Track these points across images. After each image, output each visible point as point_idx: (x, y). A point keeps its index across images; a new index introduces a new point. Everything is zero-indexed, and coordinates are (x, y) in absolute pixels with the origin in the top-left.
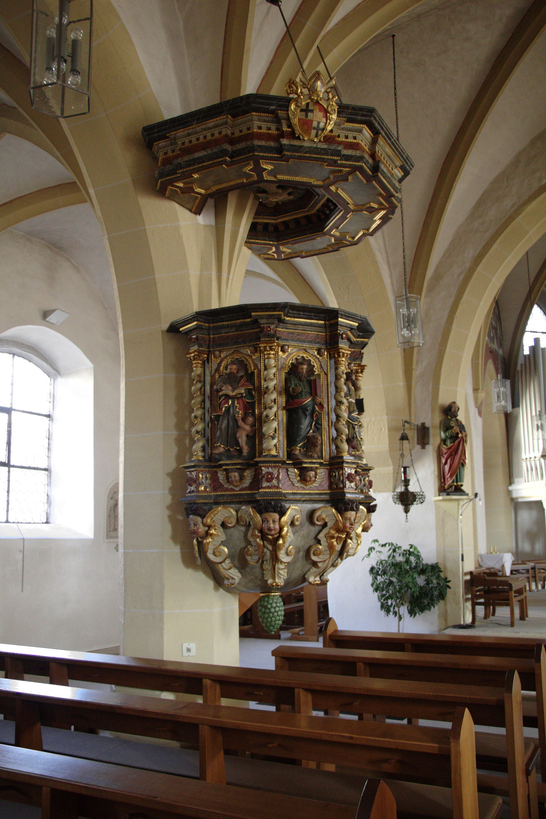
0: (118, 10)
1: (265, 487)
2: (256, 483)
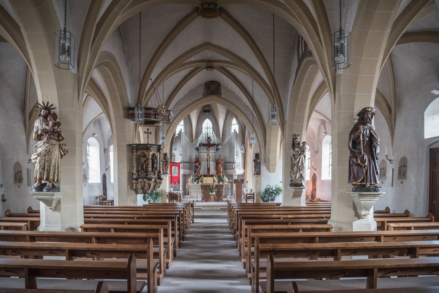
0: (57, 12)
1: (149, 176)
2: (147, 175)
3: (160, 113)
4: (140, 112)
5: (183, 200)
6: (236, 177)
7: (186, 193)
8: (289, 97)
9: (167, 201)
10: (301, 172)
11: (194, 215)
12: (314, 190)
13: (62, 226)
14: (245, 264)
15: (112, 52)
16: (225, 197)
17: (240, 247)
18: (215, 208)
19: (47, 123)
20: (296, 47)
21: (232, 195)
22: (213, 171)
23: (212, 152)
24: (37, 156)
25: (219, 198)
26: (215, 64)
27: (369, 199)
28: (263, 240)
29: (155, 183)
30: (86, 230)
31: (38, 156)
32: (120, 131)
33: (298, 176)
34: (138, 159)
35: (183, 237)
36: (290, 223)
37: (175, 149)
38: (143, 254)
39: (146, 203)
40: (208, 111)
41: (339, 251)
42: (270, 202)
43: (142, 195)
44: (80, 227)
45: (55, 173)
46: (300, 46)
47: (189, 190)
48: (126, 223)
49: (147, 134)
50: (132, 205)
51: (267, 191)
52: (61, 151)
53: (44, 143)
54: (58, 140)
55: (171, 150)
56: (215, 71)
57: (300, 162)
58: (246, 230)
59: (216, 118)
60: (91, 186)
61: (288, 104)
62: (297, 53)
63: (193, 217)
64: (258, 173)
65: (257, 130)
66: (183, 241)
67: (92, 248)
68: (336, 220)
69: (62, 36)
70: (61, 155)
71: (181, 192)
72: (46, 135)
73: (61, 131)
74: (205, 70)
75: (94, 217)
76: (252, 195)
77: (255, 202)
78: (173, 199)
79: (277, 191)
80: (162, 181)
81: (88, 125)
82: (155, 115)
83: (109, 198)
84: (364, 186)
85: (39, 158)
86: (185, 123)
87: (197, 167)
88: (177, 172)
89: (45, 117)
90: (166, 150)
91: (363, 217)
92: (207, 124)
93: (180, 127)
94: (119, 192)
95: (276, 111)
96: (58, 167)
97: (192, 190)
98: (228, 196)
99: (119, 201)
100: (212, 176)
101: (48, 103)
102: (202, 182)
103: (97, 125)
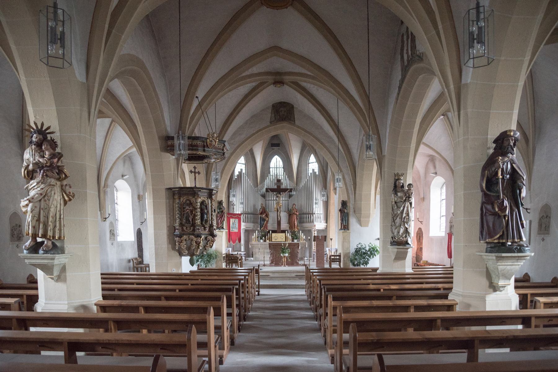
1: (197, 232)
2: (194, 230)
3: (211, 144)
4: (182, 142)
5: (245, 264)
6: (316, 232)
7: (249, 254)
8: (389, 122)
9: (224, 266)
10: (406, 226)
11: (260, 284)
12: (420, 249)
13: (68, 304)
14: (333, 357)
15: (141, 57)
16: (302, 259)
17: (325, 332)
18: (288, 275)
19: (42, 153)
20: (399, 51)
21: (310, 256)
22: (284, 225)
23: (283, 199)
24: (27, 202)
25: (293, 261)
26: (287, 78)
27: (511, 264)
28: (362, 325)
29: (205, 242)
30: (103, 308)
31: (30, 202)
32: (155, 172)
33: (402, 230)
34: (182, 208)
35: (245, 316)
36: (395, 297)
37: (234, 196)
38: (180, 348)
39: (195, 268)
40: (278, 145)
41: (476, 342)
42: (362, 266)
43: (189, 258)
44: (95, 305)
45: (55, 226)
46: (405, 48)
47: (254, 251)
48: (163, 298)
49: (193, 174)
50: (175, 271)
51: (357, 251)
52: (65, 195)
53: (38, 183)
54: (59, 179)
55: (229, 197)
56: (286, 87)
57: (404, 212)
58: (335, 308)
59: (287, 154)
60: (121, 245)
61: (388, 131)
62: (399, 59)
63: (259, 287)
64: (345, 226)
65: (343, 169)
66: (245, 321)
67: (103, 340)
68: (461, 293)
69: (51, 16)
70: (65, 200)
71: (242, 253)
72: (40, 171)
73: (63, 166)
74: (272, 85)
75: (120, 290)
76: (338, 257)
77: (342, 266)
78: (232, 263)
79: (372, 252)
80: (216, 238)
81: (115, 163)
82: (204, 147)
83: (145, 262)
84: (504, 244)
85: (30, 205)
86: (246, 160)
87: (264, 220)
88: (237, 226)
89: (39, 145)
90: (221, 196)
91: (501, 289)
92: (276, 162)
93: (240, 166)
94: (157, 254)
95: (372, 141)
96: (60, 218)
97: (257, 250)
98: (306, 258)
99: (157, 265)
100: (283, 232)
101: (42, 125)
102: (270, 239)
103: (128, 164)
